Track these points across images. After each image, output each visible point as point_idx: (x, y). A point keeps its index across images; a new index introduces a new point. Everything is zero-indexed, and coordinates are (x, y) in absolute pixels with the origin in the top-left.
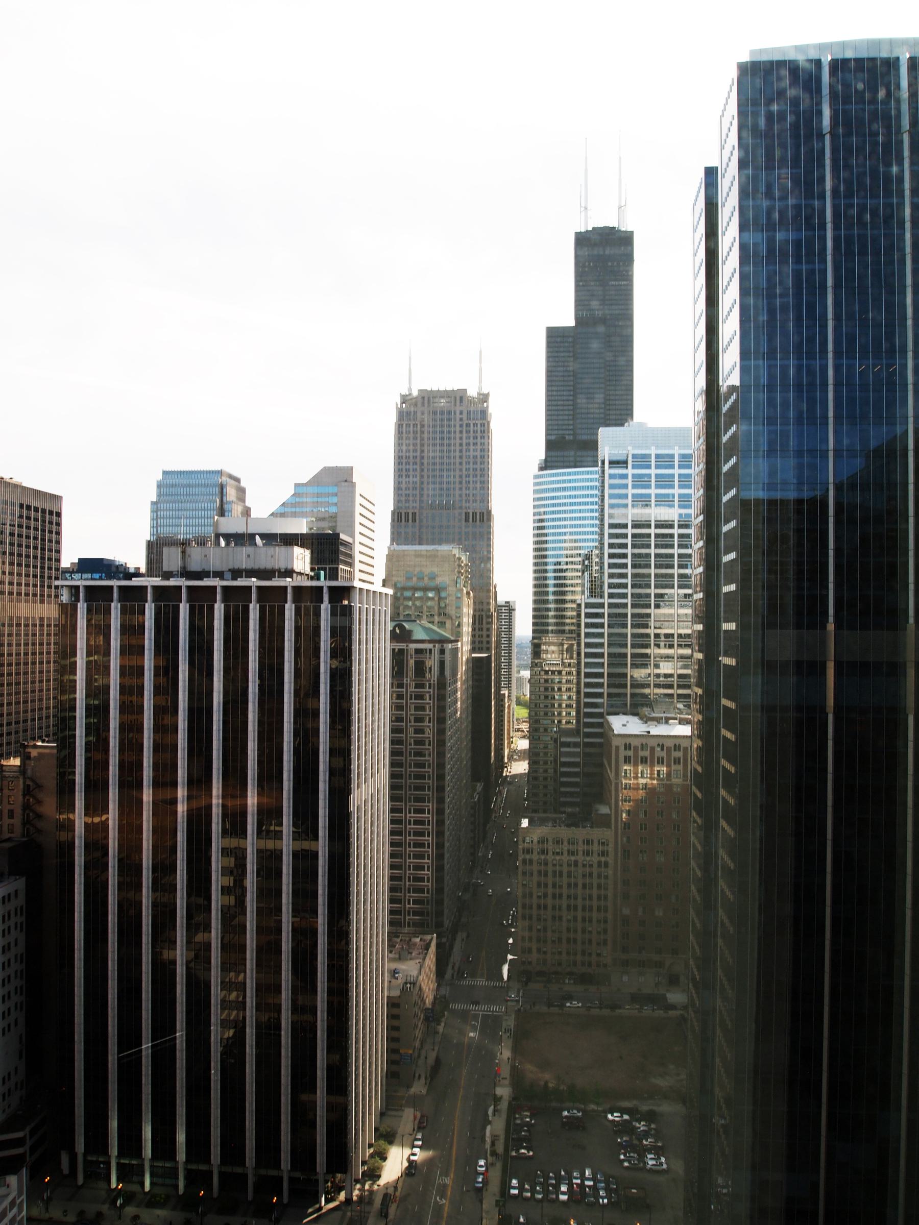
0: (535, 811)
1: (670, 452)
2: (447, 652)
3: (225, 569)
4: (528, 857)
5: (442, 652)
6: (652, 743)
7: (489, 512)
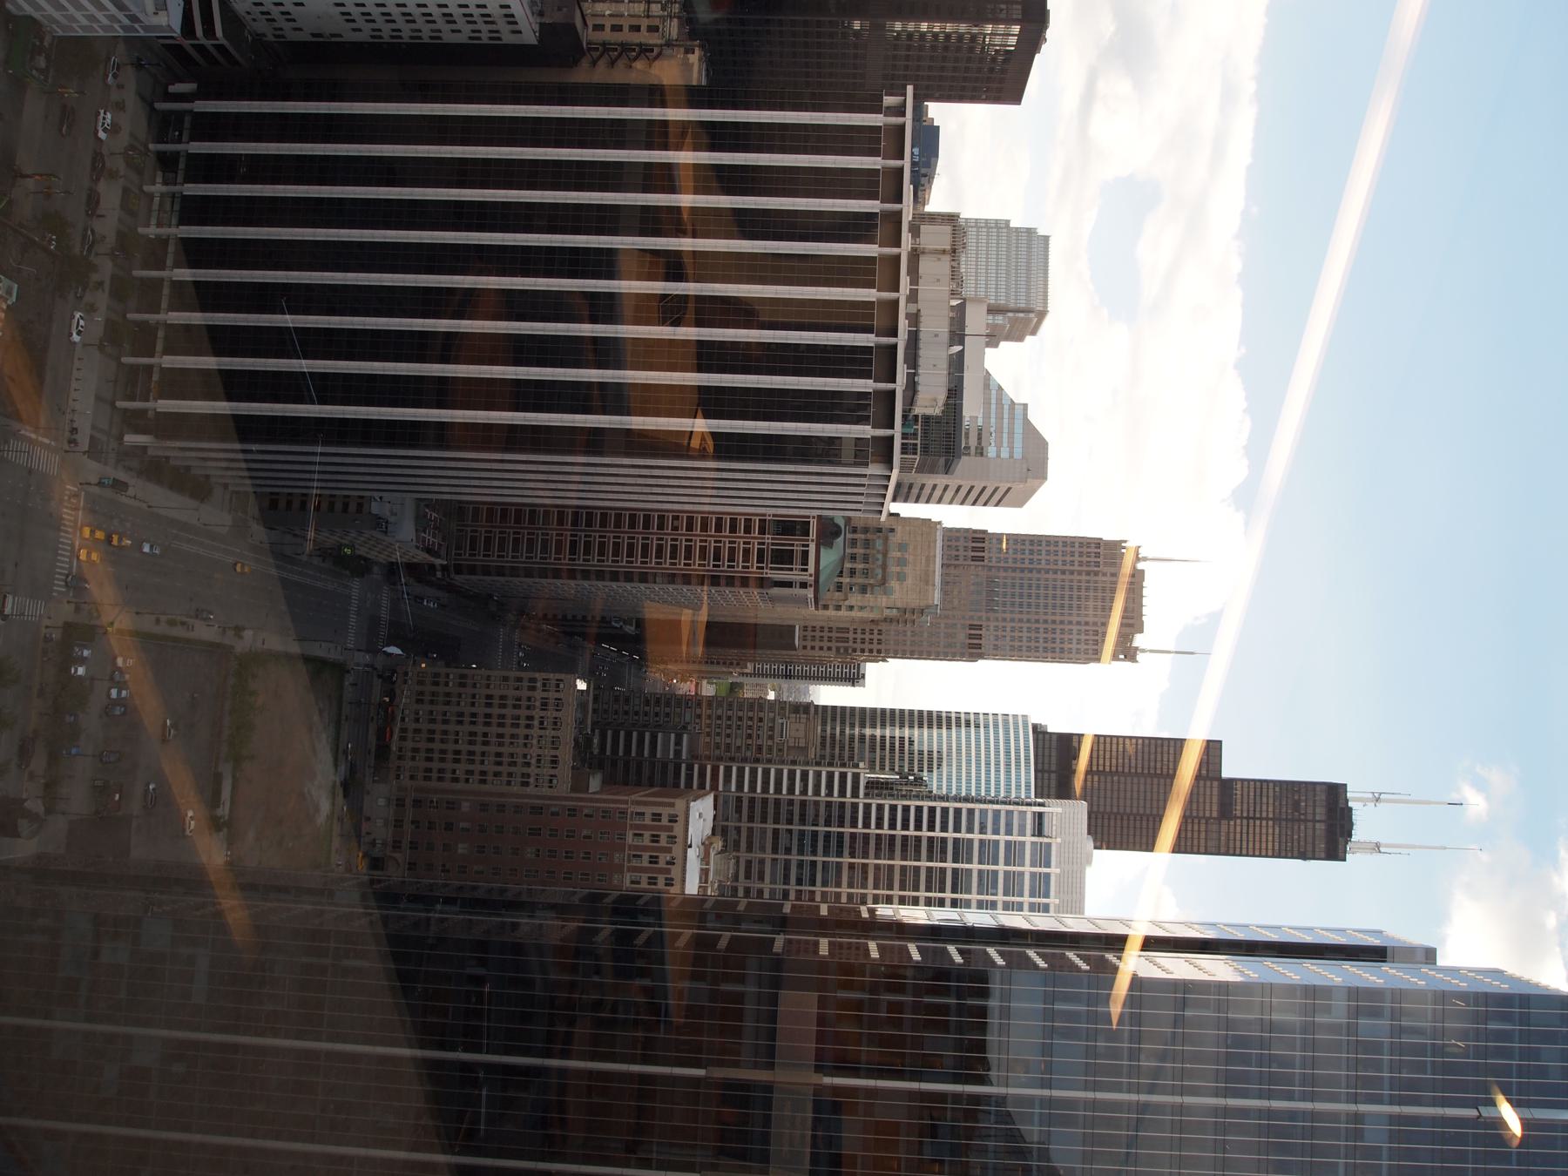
0: (596, 699)
1: (1052, 893)
2: (803, 591)
3: (920, 305)
4: (539, 684)
5: (804, 585)
6: (677, 850)
7: (981, 656)
